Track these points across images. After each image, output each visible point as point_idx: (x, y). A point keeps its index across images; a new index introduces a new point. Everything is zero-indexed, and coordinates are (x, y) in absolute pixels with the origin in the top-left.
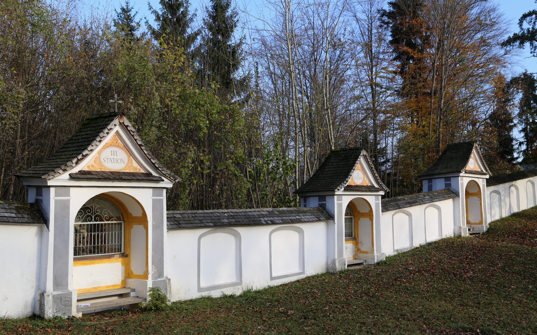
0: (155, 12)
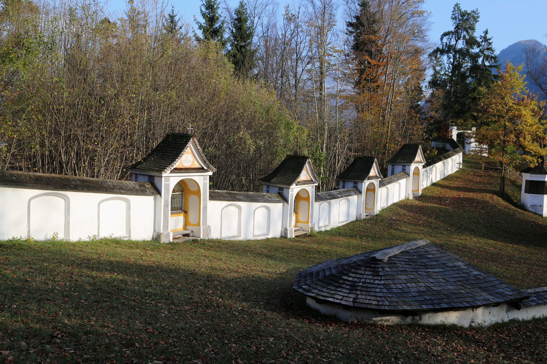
0: (198, 23)
